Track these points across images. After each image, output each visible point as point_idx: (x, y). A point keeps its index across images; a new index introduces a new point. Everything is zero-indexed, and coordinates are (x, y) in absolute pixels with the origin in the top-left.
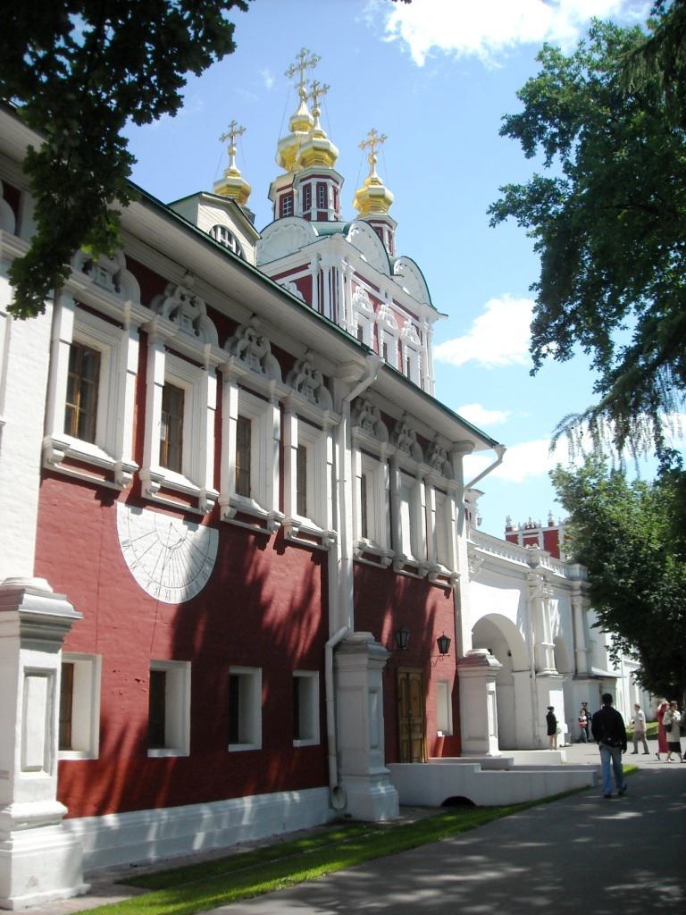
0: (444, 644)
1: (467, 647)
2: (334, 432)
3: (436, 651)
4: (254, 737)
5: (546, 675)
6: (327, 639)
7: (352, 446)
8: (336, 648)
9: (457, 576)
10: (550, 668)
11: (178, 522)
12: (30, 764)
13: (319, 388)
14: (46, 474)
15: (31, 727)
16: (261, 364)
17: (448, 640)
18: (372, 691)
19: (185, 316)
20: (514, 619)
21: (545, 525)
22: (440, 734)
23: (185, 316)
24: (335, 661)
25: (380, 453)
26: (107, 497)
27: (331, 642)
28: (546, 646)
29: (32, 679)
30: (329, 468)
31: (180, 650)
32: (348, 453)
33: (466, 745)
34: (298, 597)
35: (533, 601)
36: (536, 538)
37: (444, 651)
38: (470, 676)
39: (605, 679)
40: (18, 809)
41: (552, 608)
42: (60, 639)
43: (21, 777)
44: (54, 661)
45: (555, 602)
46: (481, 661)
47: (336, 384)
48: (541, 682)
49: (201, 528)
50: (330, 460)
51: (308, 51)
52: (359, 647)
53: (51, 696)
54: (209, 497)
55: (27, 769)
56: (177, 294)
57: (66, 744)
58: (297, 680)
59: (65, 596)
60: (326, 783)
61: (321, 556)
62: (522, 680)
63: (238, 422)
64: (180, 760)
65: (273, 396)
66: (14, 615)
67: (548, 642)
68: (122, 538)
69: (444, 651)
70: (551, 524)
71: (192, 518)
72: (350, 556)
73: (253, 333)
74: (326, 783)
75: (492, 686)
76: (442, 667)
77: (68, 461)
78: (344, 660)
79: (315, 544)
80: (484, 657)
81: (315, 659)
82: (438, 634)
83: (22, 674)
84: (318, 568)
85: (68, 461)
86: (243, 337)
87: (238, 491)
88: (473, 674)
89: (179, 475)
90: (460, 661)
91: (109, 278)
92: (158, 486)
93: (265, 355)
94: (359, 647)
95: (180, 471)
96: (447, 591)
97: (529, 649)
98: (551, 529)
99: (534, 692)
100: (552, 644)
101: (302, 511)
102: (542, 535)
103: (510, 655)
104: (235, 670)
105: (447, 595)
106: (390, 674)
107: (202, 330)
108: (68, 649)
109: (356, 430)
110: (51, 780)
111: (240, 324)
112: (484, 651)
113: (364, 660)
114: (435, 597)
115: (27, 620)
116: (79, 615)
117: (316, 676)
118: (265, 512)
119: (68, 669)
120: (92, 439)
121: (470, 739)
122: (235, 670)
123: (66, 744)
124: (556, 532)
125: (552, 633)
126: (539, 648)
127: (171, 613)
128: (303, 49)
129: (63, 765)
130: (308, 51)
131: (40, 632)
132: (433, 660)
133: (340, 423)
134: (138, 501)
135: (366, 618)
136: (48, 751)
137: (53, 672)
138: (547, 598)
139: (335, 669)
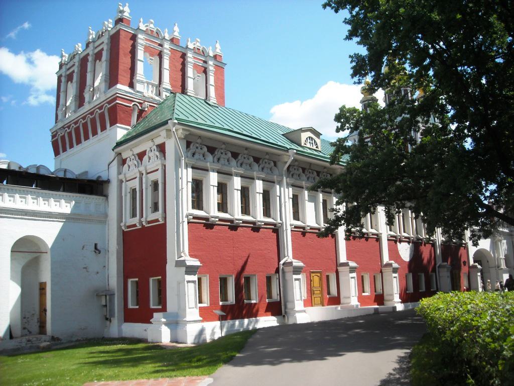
0: (465, 263)
1: (472, 262)
2: (280, 183)
3: (462, 265)
4: (424, 289)
5: (502, 269)
7: (288, 185)
8: (439, 267)
9: (467, 243)
10: (503, 266)
11: (407, 244)
12: (190, 307)
13: (272, 167)
14: (388, 240)
15: (206, 294)
16: (250, 166)
17: (466, 262)
18: (448, 277)
20: (488, 249)
22: (465, 288)
25: (231, 172)
26: (396, 242)
27: (437, 265)
28: (501, 258)
29: (189, 284)
30: (278, 198)
31: (410, 271)
32: (286, 190)
33: (342, 301)
34: (429, 257)
35: (496, 242)
37: (465, 265)
38: (472, 270)
40: (187, 319)
41: (503, 243)
42: (301, 271)
43: (296, 302)
44: (195, 278)
45: (505, 241)
46: (476, 267)
47: (279, 164)
48: (500, 271)
49: (411, 244)
50: (278, 194)
52: (444, 267)
53: (195, 288)
54: (279, 224)
55: (189, 308)
57: (200, 302)
61: (434, 245)
62: (493, 271)
64: (423, 292)
65: (209, 168)
66: (391, 268)
67: (502, 256)
69: (465, 265)
71: (409, 243)
72: (440, 243)
75: (479, 274)
76: (464, 270)
77: (194, 218)
78: (441, 270)
79: (273, 227)
80: (476, 265)
81: (434, 270)
82: (462, 260)
83: (186, 282)
84: (433, 248)
85: (194, 218)
89: (130, 38)
90: (469, 267)
92: (192, 217)
94: (444, 267)
95: (299, 220)
96: (465, 247)
97: (495, 260)
99: (497, 274)
100: (504, 257)
101: (404, 232)
103: (488, 262)
105: (465, 249)
106: (451, 272)
108: (199, 274)
109: (288, 179)
110: (197, 311)
111: (261, 159)
112: (477, 264)
113: (446, 270)
114: (462, 251)
115: (394, 269)
116: (400, 267)
118: (421, 238)
119: (199, 279)
120: (226, 212)
121: (387, 295)
123: (200, 302)
125: (503, 253)
126: (499, 259)
127: (407, 263)
129: (200, 308)
131: (191, 270)
132: (462, 267)
133: (283, 178)
134: (400, 241)
135: (445, 259)
136: (196, 304)
137: (195, 281)
138: (501, 241)
139: (439, 272)
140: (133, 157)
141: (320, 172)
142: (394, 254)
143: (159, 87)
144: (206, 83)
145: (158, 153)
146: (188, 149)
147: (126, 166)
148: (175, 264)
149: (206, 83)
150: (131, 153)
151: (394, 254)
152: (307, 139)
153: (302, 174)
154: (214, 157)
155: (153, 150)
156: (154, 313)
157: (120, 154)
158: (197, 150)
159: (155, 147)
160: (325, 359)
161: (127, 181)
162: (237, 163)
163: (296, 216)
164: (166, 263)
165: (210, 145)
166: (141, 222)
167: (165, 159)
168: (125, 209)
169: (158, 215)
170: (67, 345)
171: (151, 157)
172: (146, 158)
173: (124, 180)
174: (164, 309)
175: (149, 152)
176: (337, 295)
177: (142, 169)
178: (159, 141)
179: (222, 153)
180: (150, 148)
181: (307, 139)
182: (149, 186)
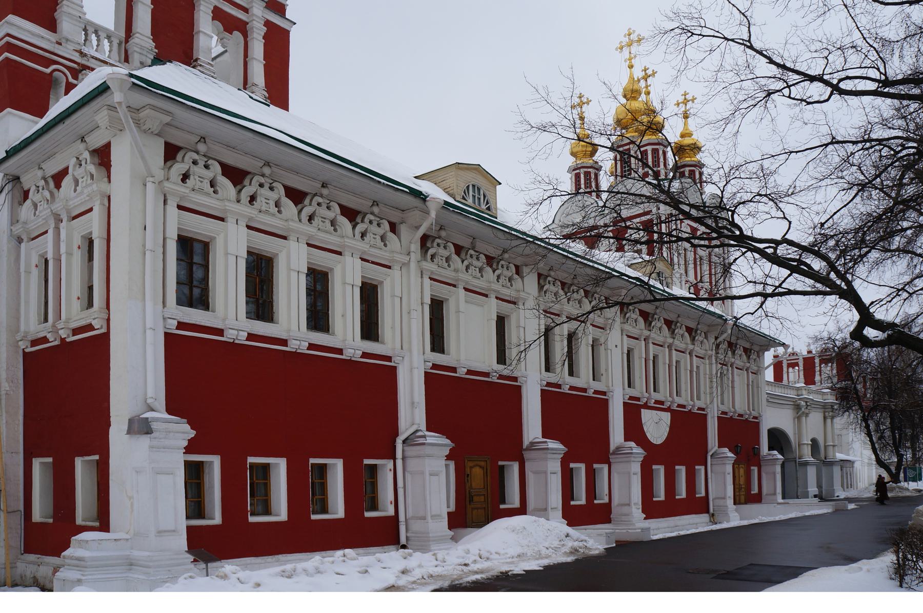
6: (397, 435)
19: (322, 218)
21: (805, 353)
23: (373, 234)
24: (403, 451)
36: (797, 362)
39: (845, 462)
51: (634, 31)
56: (366, 220)
58: (503, 467)
59: (185, 420)
60: (707, 511)
63: (361, 288)
68: (643, 422)
70: (810, 352)
73: (262, 180)
74: (707, 511)
86: (362, 221)
87: (433, 350)
88: (620, 460)
89: (442, 355)
91: (328, 224)
93: (279, 199)
98: (810, 355)
102: (802, 360)
104: (500, 463)
107: (388, 241)
117: (703, 468)
122: (500, 463)
124: (813, 358)
128: (630, 29)
130: (634, 31)
140: (42, 183)
141: (493, 258)
142: (634, 430)
143: (127, 41)
144: (246, 55)
145: (92, 168)
146: (169, 163)
147: (28, 202)
148: (126, 427)
149: (246, 55)
150: (40, 173)
151: (634, 430)
152: (468, 187)
153: (455, 257)
154: (240, 191)
155: (83, 163)
156: (287, 520)
157: (18, 178)
158: (195, 169)
159: (86, 155)
160: (524, 571)
161: (33, 239)
162: (300, 212)
163: (438, 343)
164: (110, 425)
165: (233, 160)
166: (55, 330)
167: (110, 181)
168: (27, 302)
169: (94, 317)
170: (737, 474)
171: (80, 181)
172: (67, 182)
173: (24, 237)
174: (104, 526)
175: (74, 166)
176: (394, 514)
177: (57, 206)
178: (96, 141)
179: (261, 185)
180: (78, 158)
181: (468, 187)
182: (76, 247)
